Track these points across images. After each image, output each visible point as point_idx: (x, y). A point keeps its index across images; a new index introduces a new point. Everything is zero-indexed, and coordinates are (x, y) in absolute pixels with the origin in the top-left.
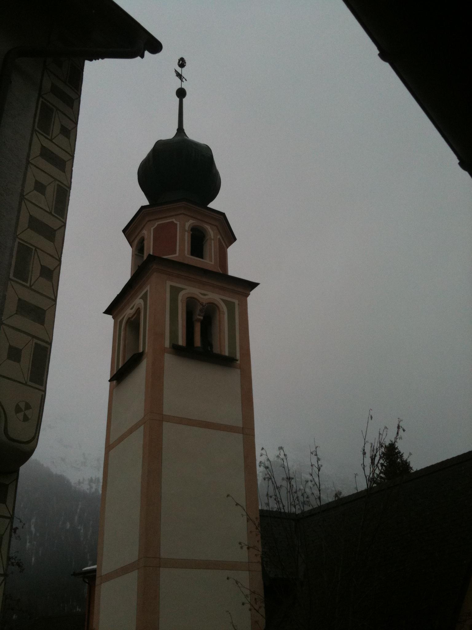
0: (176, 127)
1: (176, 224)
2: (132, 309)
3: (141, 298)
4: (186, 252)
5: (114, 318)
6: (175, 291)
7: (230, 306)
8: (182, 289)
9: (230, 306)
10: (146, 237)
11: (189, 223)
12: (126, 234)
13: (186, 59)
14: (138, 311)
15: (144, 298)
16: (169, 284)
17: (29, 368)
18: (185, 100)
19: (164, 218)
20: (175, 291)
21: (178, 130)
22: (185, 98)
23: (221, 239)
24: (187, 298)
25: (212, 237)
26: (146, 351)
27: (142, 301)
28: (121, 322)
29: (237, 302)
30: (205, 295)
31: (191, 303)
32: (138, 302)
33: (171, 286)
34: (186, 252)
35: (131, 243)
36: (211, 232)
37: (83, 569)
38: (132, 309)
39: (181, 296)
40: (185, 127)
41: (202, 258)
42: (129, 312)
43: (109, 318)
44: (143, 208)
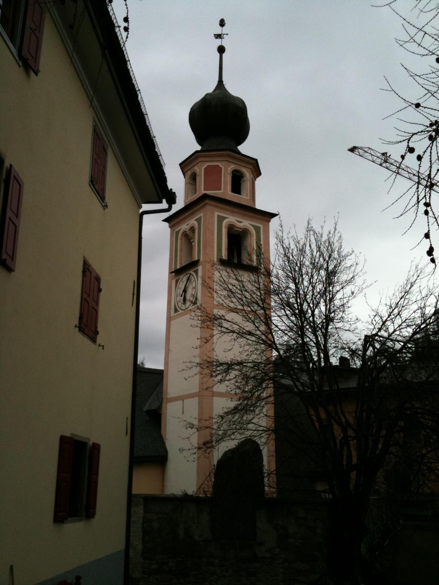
0: (217, 79)
1: (260, 228)
2: (187, 225)
3: (196, 220)
4: (229, 191)
5: (170, 227)
6: (221, 219)
7: (257, 229)
8: (226, 218)
9: (257, 229)
10: (198, 173)
11: (232, 167)
12: (185, 171)
13: (226, 21)
14: (192, 229)
15: (199, 220)
16: (216, 214)
17: (181, 281)
18: (224, 55)
19: (211, 161)
20: (221, 219)
21: (219, 82)
22: (224, 53)
23: (253, 177)
24: (229, 225)
25: (248, 179)
26: (201, 260)
27: (196, 224)
28: (177, 233)
29: (261, 226)
30: (240, 222)
31: (231, 228)
32: (192, 222)
33: (218, 216)
34: (229, 191)
35: (184, 174)
36: (247, 174)
37: (369, 343)
38: (187, 225)
39: (225, 223)
40: (224, 79)
41: (240, 193)
42: (184, 227)
43: (166, 224)
44: (197, 152)
